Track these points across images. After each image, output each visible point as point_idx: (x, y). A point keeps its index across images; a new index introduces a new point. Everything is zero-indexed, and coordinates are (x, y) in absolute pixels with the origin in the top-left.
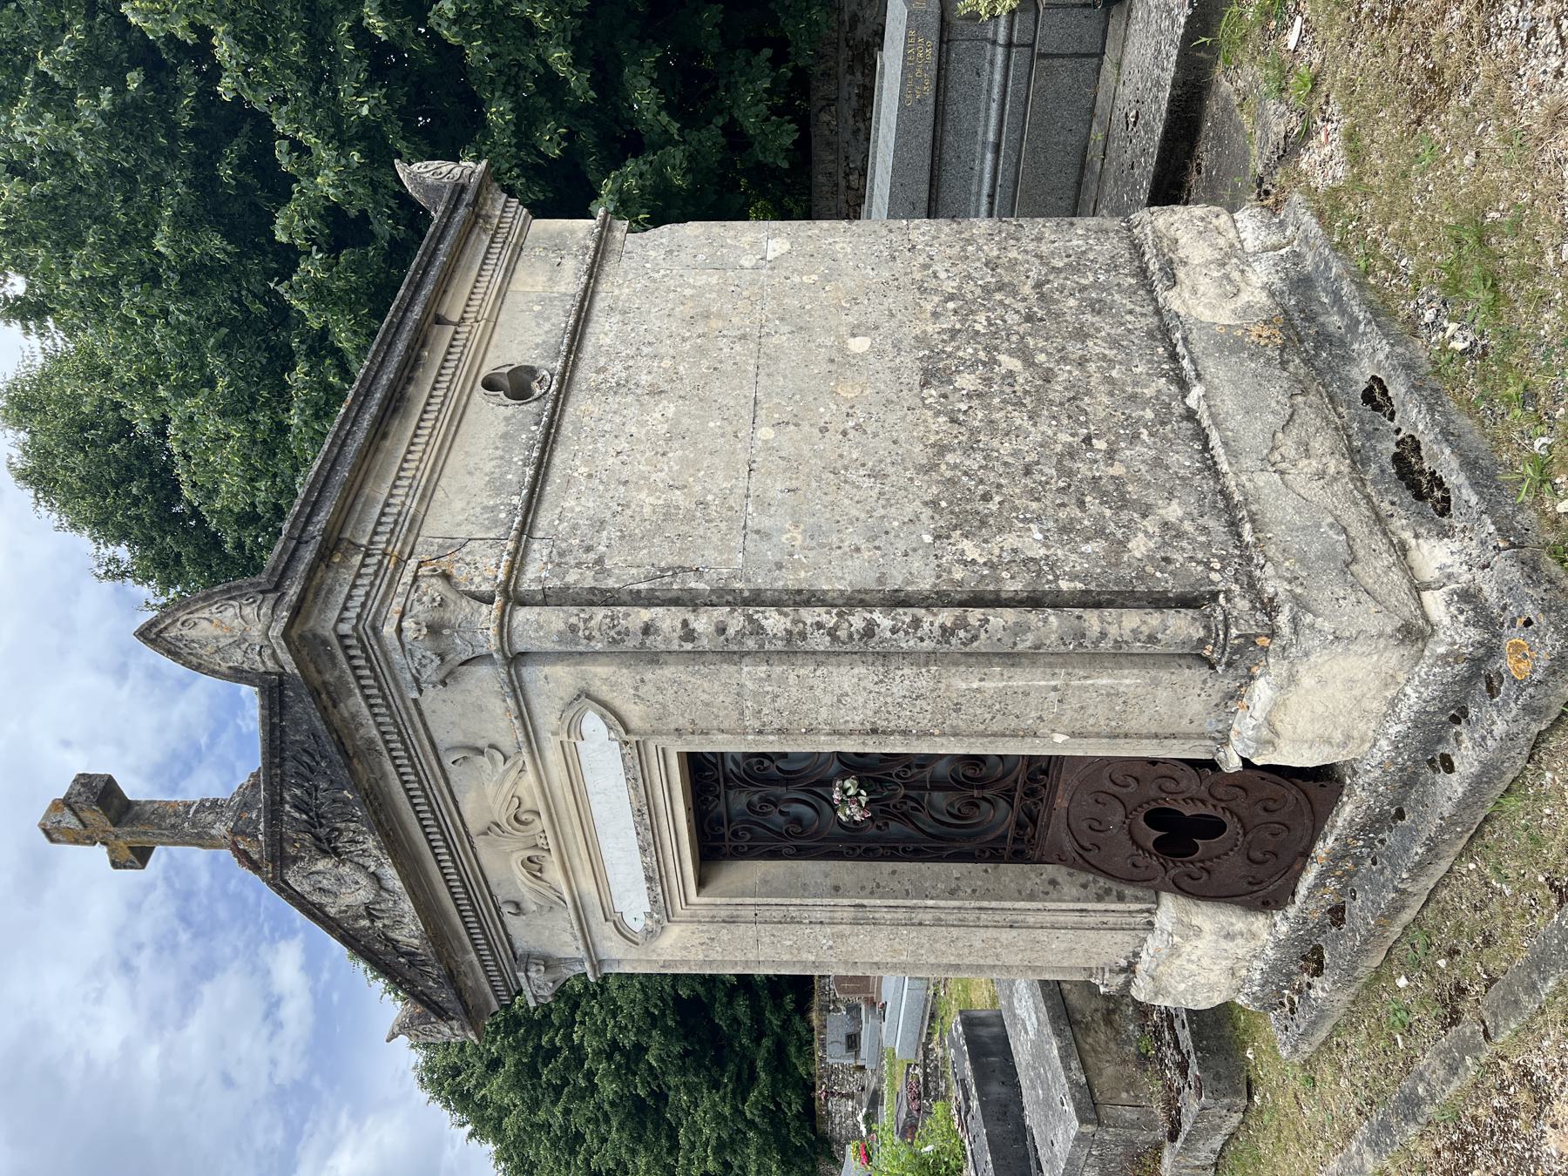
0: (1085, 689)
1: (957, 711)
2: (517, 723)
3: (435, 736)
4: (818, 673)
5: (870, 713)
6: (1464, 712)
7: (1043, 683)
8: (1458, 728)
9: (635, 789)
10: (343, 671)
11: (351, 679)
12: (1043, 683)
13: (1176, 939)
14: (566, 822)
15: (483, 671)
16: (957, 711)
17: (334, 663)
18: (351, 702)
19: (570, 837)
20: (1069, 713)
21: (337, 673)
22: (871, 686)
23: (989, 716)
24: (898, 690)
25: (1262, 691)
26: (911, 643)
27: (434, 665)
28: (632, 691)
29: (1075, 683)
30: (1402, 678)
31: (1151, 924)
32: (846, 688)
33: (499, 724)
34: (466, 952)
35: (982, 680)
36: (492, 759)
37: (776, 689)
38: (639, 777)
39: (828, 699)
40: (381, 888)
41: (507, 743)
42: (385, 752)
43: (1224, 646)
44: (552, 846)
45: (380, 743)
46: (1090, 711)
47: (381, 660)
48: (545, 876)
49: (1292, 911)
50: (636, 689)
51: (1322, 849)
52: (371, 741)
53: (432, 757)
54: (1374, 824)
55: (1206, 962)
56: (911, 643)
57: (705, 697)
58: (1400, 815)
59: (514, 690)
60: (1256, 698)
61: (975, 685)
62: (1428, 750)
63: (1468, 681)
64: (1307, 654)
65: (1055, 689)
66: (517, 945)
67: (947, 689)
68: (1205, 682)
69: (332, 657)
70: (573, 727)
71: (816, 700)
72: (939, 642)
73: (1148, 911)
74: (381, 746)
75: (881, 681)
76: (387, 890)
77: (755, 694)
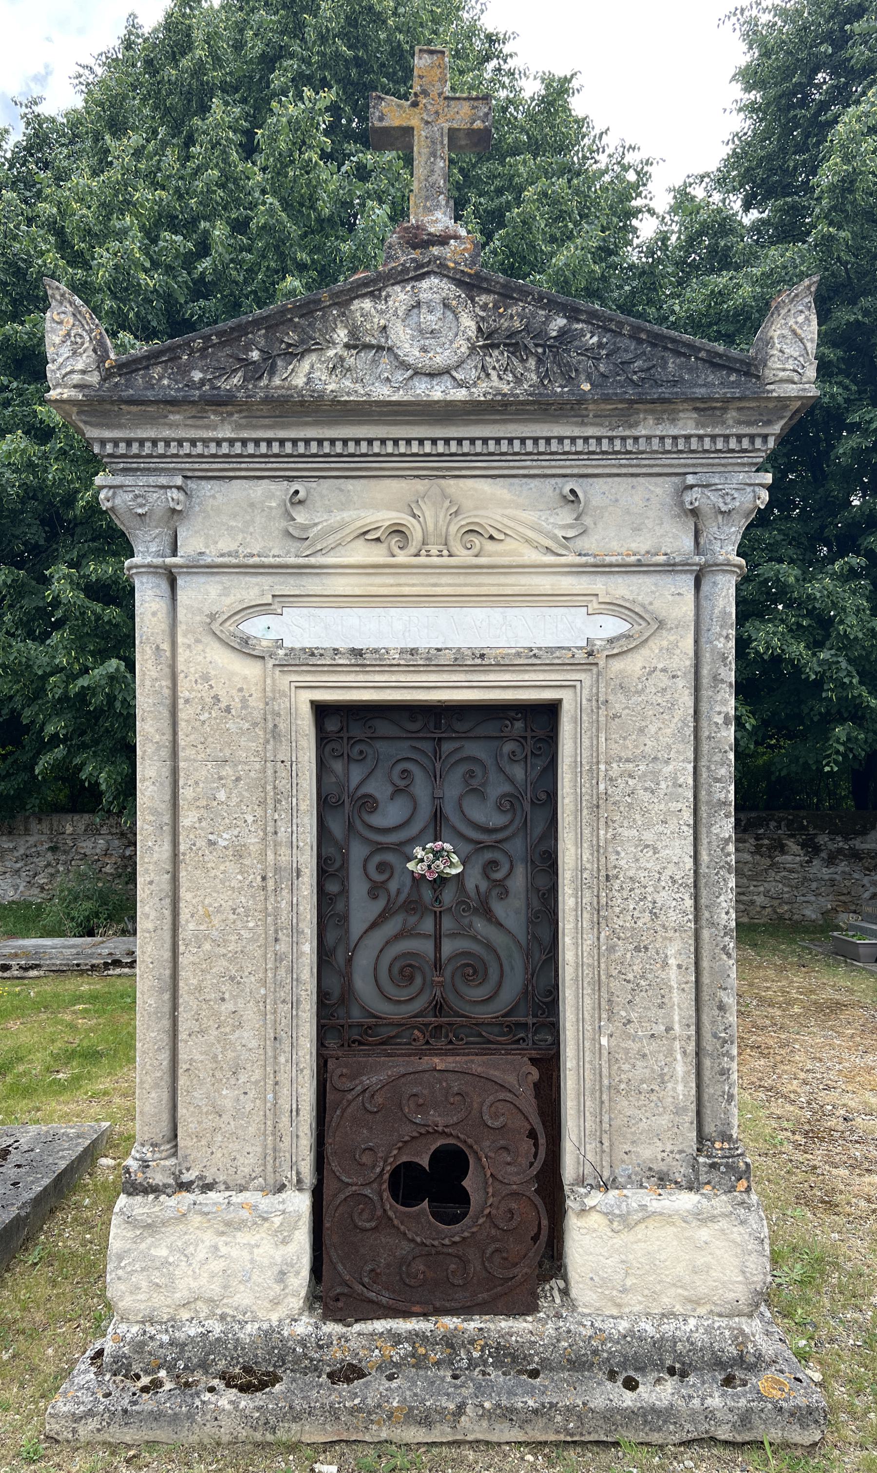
0: (670, 1052)
1: (637, 949)
2: (633, 559)
3: (601, 480)
4: (685, 828)
5: (631, 873)
6: (684, 1375)
7: (676, 1018)
8: (667, 1377)
9: (518, 655)
10: (728, 427)
11: (717, 431)
12: (676, 1018)
13: (277, 1221)
14: (461, 580)
15: (688, 543)
16: (637, 949)
17: (739, 423)
18: (691, 423)
19: (434, 580)
20: (636, 1046)
21: (731, 422)
22: (668, 873)
23: (630, 976)
24: (662, 898)
25: (687, 1200)
26: (724, 905)
27: (721, 505)
28: (660, 666)
29: (677, 1045)
30: (702, 1311)
31: (281, 1188)
32: (664, 853)
33: (609, 539)
34: (239, 427)
35: (679, 966)
36: (570, 526)
37: (662, 792)
38: (532, 659)
39: (649, 837)
40: (416, 373)
41: (589, 544)
42: (610, 434)
43: (733, 1156)
44: (422, 560)
45: (627, 433)
46: (639, 1064)
47: (723, 461)
48: (360, 542)
49: (332, 1328)
50: (664, 670)
51: (450, 1322)
52: (636, 424)
53: (576, 471)
54: (512, 1359)
55: (217, 1266)
56: (724, 905)
57: (652, 729)
58: (534, 1374)
59: (674, 565)
60: (673, 1198)
61: (672, 961)
62: (630, 1364)
63: (718, 1363)
64: (742, 1223)
65: (668, 1029)
66: (207, 485)
67: (665, 938)
68: (681, 1152)
69: (749, 424)
70: (616, 608)
71: (648, 826)
72: (725, 927)
73: (299, 1181)
74: (621, 432)
75: (674, 882)
76: (411, 377)
77: (655, 774)
